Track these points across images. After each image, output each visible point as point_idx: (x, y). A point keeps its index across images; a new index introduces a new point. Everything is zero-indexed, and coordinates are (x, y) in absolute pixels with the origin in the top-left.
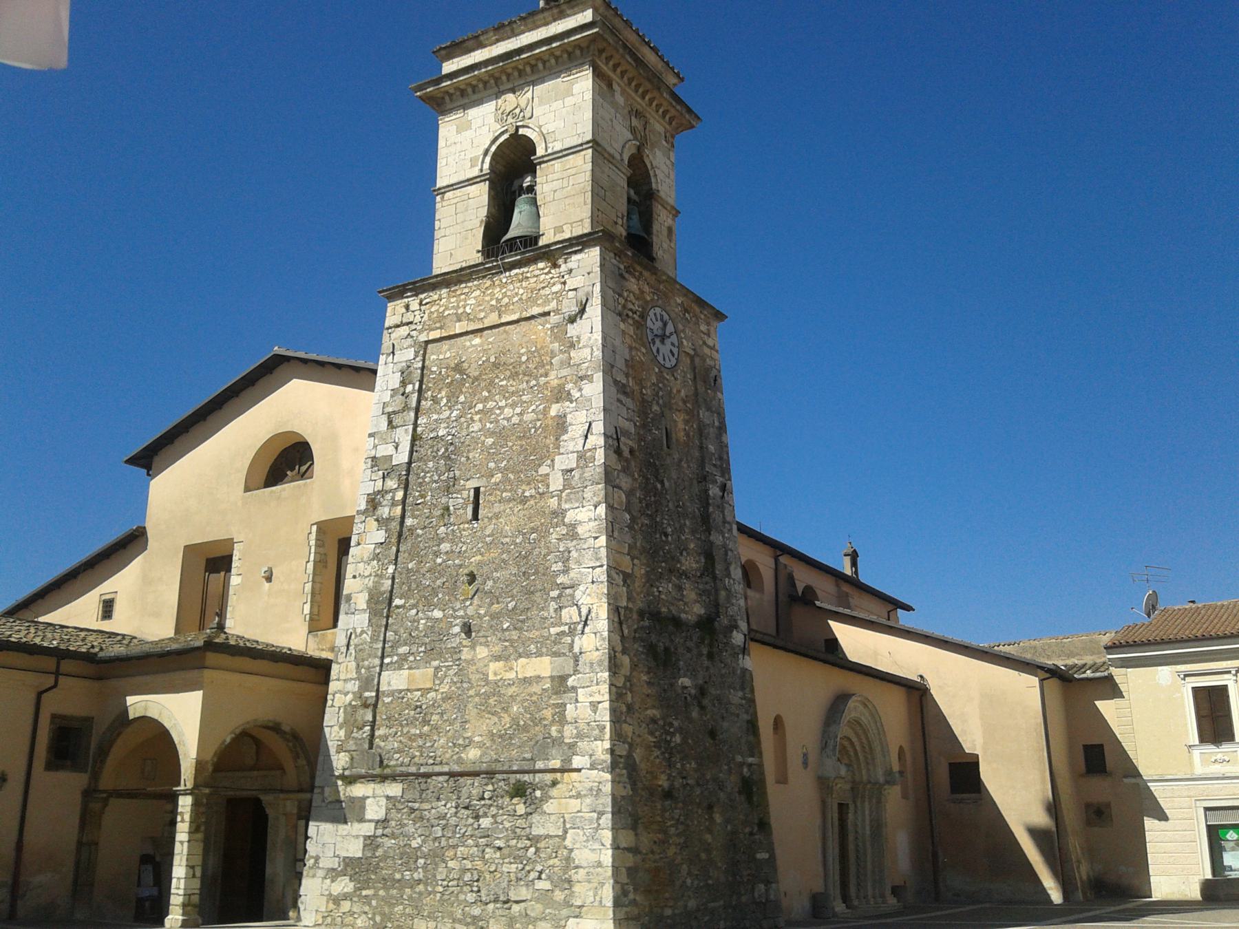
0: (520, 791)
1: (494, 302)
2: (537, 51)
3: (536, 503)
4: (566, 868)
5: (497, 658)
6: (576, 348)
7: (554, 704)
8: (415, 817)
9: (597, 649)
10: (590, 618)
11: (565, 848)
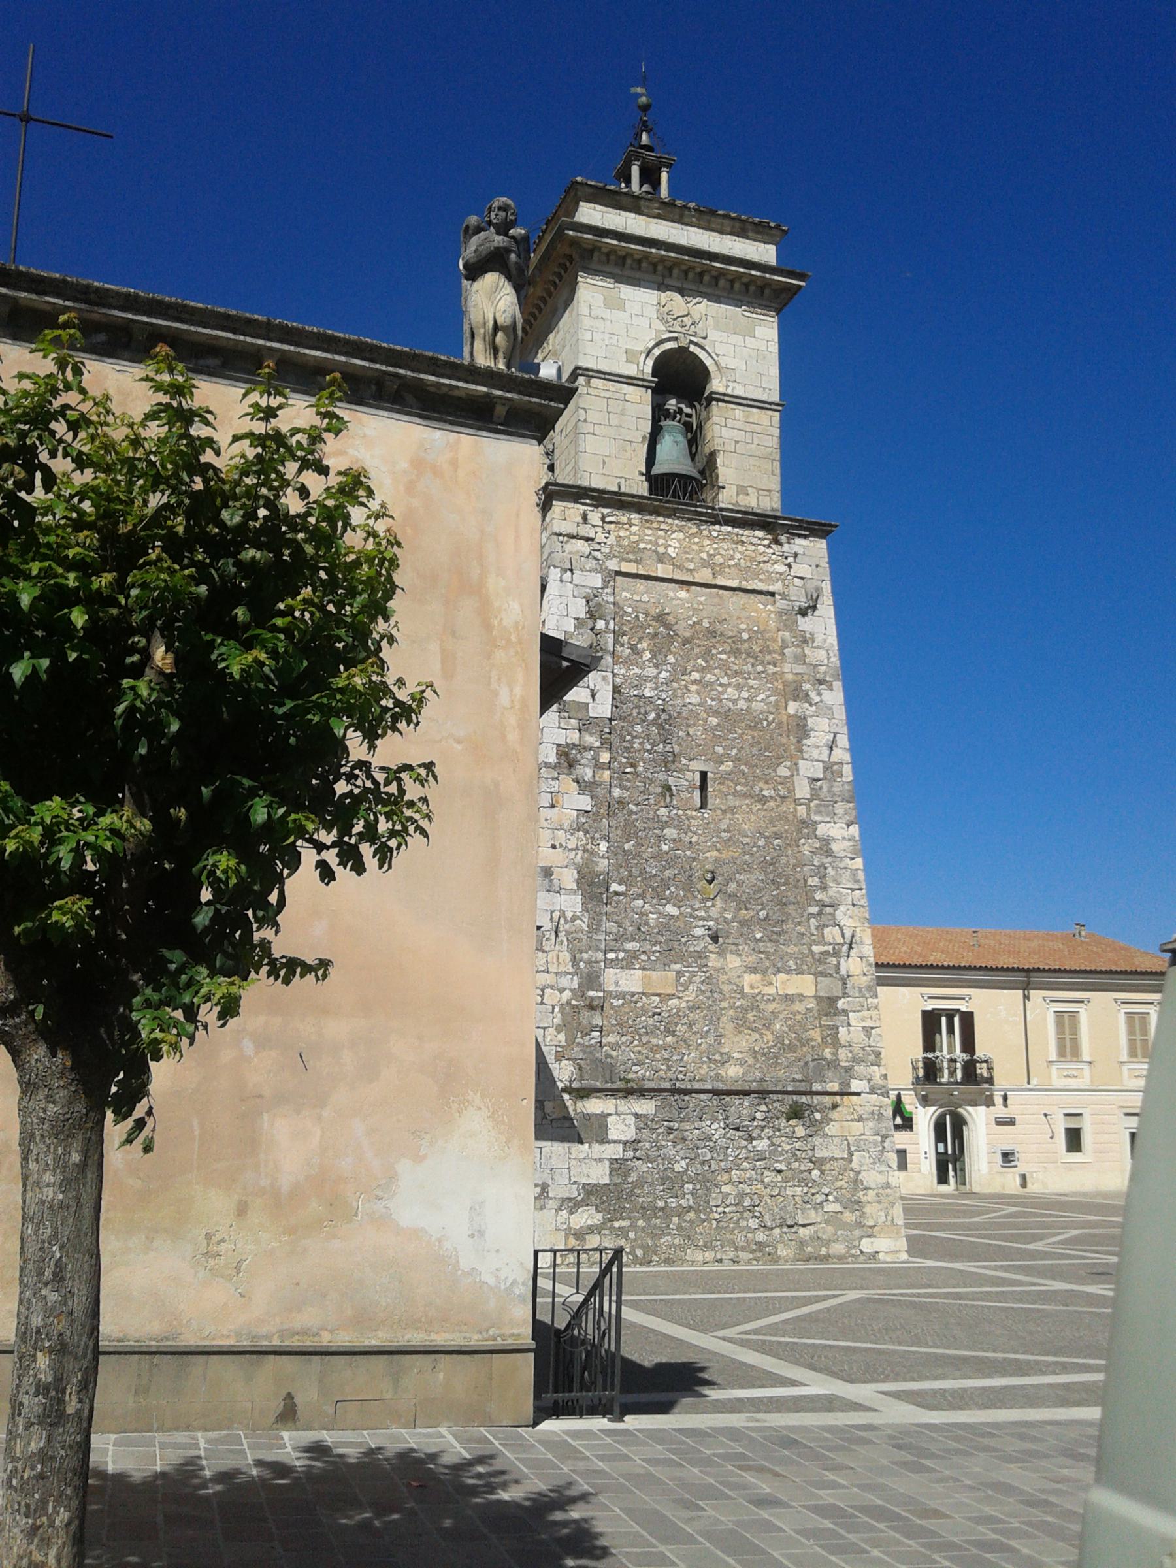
0: (796, 1113)
4: (856, 1189)
5: (754, 970)
6: (810, 645)
9: (865, 975)
11: (852, 1170)
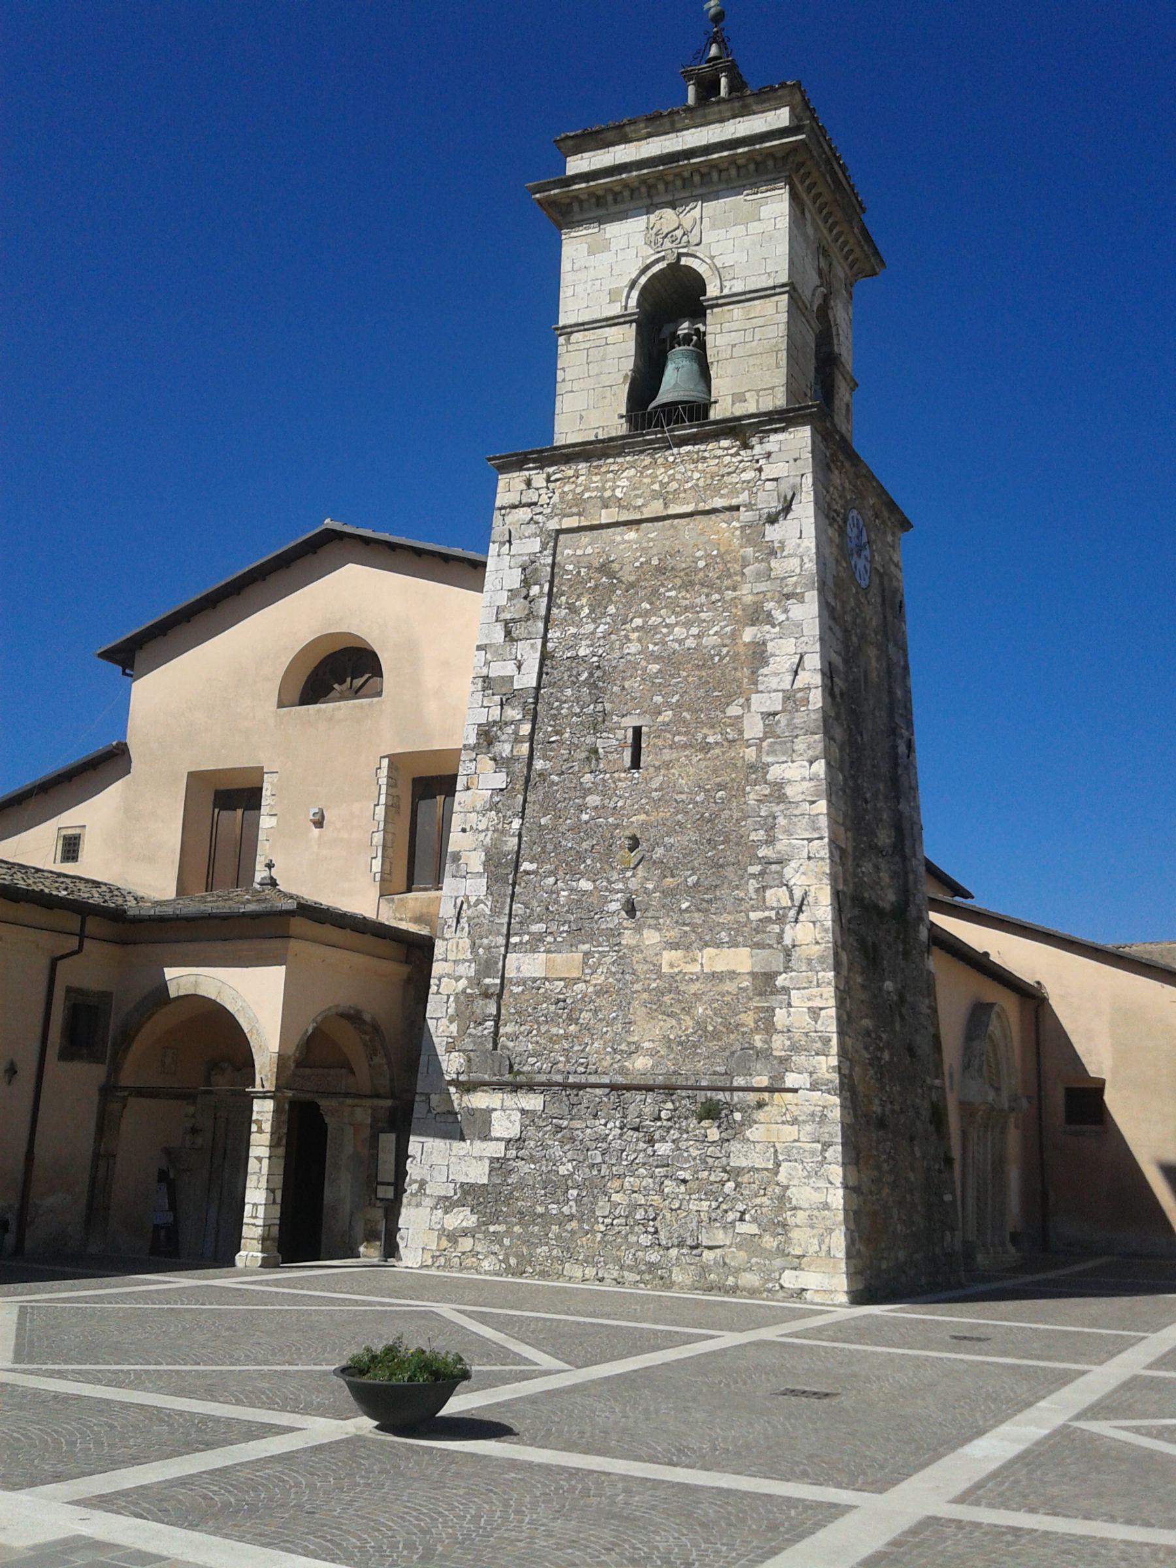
0: (711, 1112)
1: (656, 487)
3: (723, 753)
6: (779, 555)
8: (563, 1137)
9: (817, 943)
10: (805, 902)
11: (778, 1184)
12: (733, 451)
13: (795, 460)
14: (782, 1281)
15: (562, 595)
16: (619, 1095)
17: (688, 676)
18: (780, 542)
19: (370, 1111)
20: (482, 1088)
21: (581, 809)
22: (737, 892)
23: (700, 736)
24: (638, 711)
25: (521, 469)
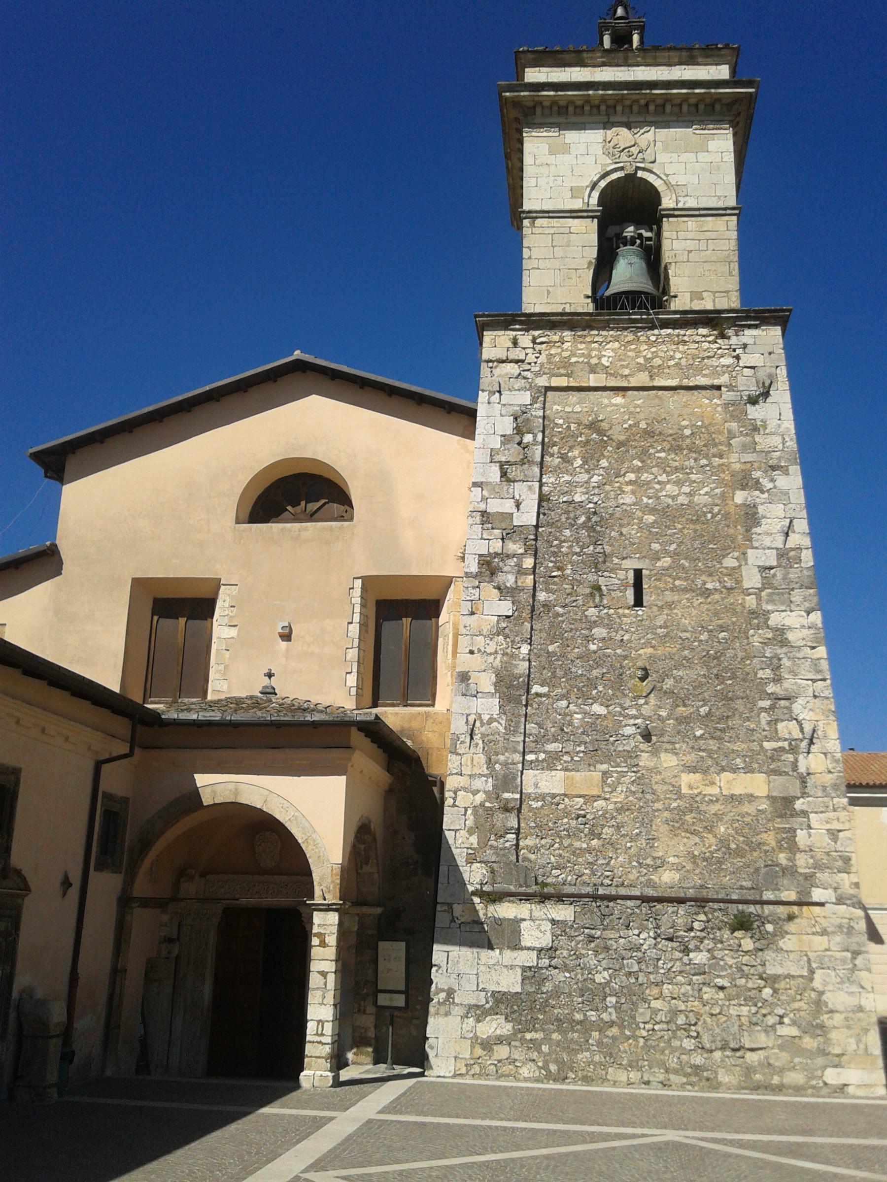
0: (743, 924)
1: (641, 360)
2: (675, 91)
3: (723, 599)
6: (762, 432)
7: (779, 828)
8: (597, 946)
9: (830, 772)
10: (815, 735)
11: (813, 990)
12: (711, 338)
13: (770, 353)
14: (824, 1078)
15: (554, 445)
16: (650, 907)
17: (684, 528)
18: (762, 421)
19: (357, 918)
20: (508, 898)
21: (588, 639)
22: (748, 723)
23: (699, 582)
24: (638, 555)
25: (506, 328)
